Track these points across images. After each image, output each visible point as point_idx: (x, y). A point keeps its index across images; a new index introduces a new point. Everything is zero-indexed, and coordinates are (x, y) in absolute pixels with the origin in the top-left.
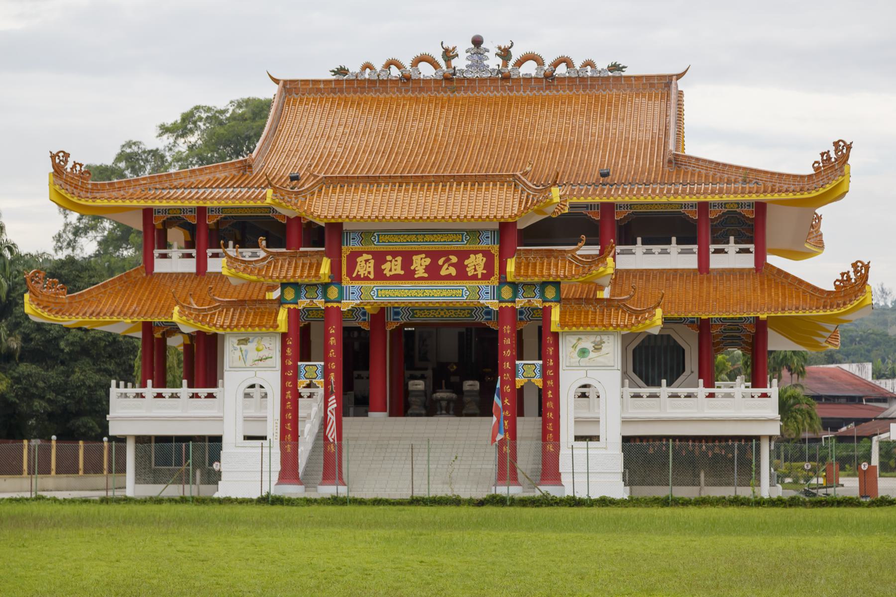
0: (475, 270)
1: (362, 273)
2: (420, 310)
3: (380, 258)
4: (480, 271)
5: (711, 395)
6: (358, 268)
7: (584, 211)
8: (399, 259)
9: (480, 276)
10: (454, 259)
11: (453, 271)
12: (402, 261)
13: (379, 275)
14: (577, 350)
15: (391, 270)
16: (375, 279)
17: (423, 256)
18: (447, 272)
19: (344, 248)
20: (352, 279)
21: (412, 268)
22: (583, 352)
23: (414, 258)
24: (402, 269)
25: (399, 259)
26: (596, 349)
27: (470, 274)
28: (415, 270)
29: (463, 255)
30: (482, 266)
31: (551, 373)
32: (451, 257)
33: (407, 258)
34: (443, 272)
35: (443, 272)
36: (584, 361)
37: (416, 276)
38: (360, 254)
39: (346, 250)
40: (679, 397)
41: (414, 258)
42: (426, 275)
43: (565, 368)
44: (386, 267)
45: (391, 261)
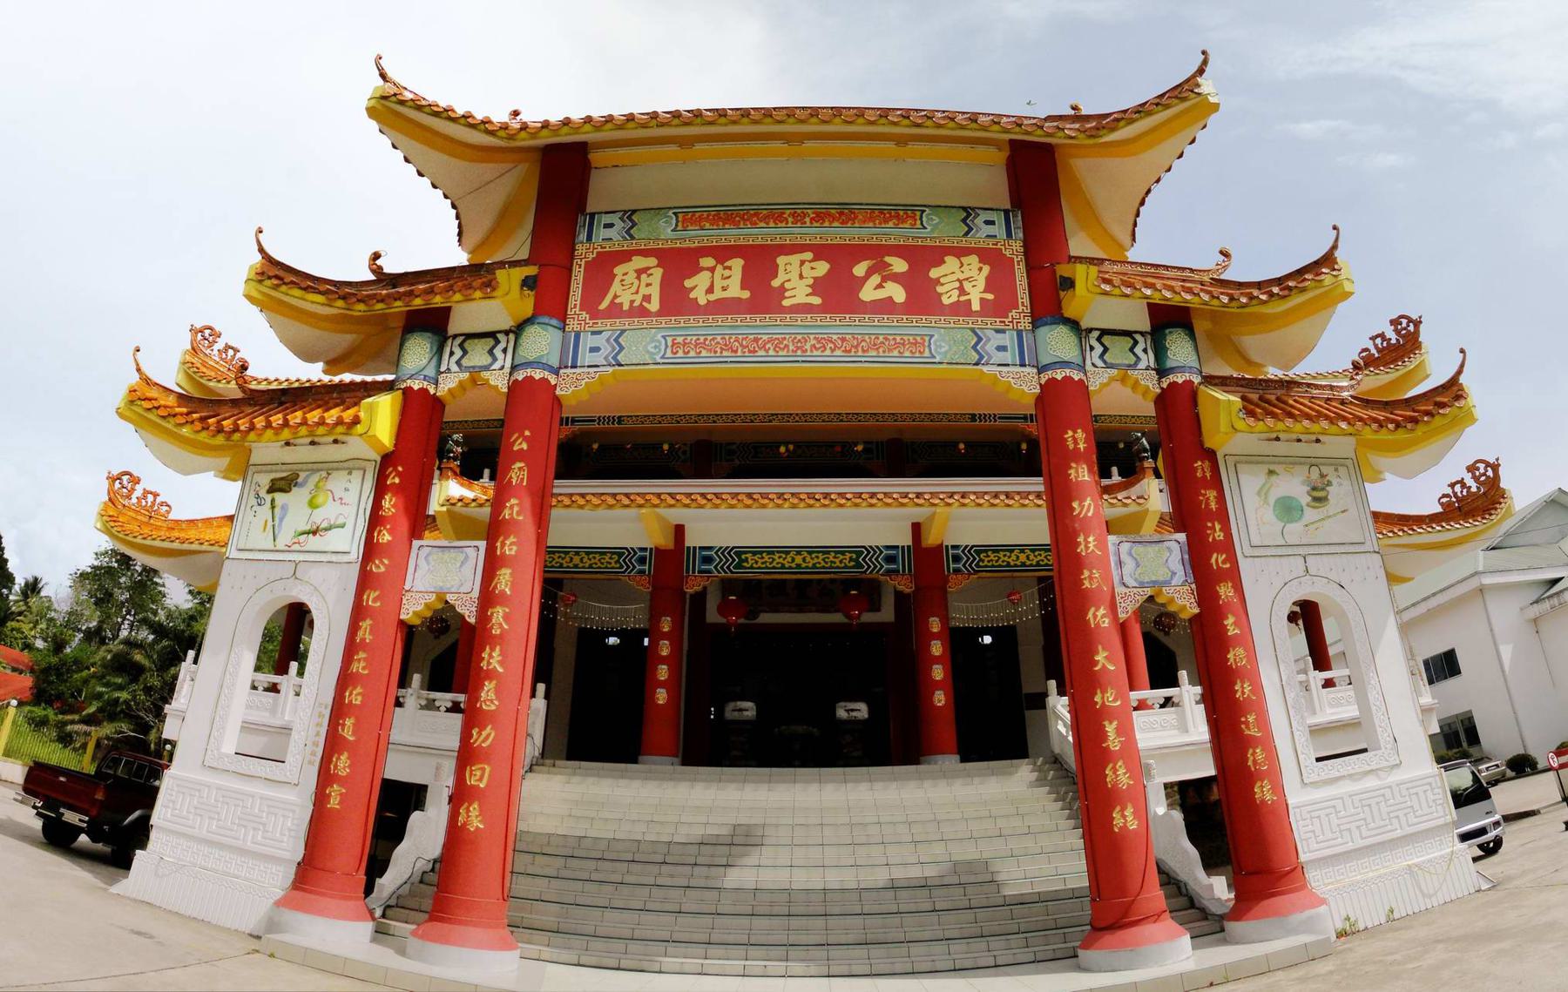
0: (962, 291)
1: (625, 300)
2: (754, 554)
3: (678, 264)
4: (976, 295)
5: (1329, 684)
6: (616, 287)
7: (1021, 424)
8: (737, 264)
9: (976, 306)
10: (899, 265)
11: (897, 293)
12: (744, 268)
13: (675, 302)
14: (1272, 501)
15: (710, 290)
16: (660, 313)
17: (808, 255)
18: (881, 294)
19: (581, 249)
20: (595, 315)
21: (776, 283)
22: (1287, 509)
23: (781, 260)
24: (743, 287)
25: (737, 264)
26: (1316, 499)
27: (946, 301)
28: (782, 289)
29: (924, 257)
30: (981, 284)
31: (1210, 564)
32: (888, 259)
33: (760, 262)
34: (868, 293)
35: (868, 293)
36: (1295, 531)
37: (786, 303)
38: (625, 256)
39: (584, 252)
40: (1151, 707)
41: (781, 260)
42: (816, 301)
43: (1248, 551)
44: (698, 286)
45: (712, 270)
